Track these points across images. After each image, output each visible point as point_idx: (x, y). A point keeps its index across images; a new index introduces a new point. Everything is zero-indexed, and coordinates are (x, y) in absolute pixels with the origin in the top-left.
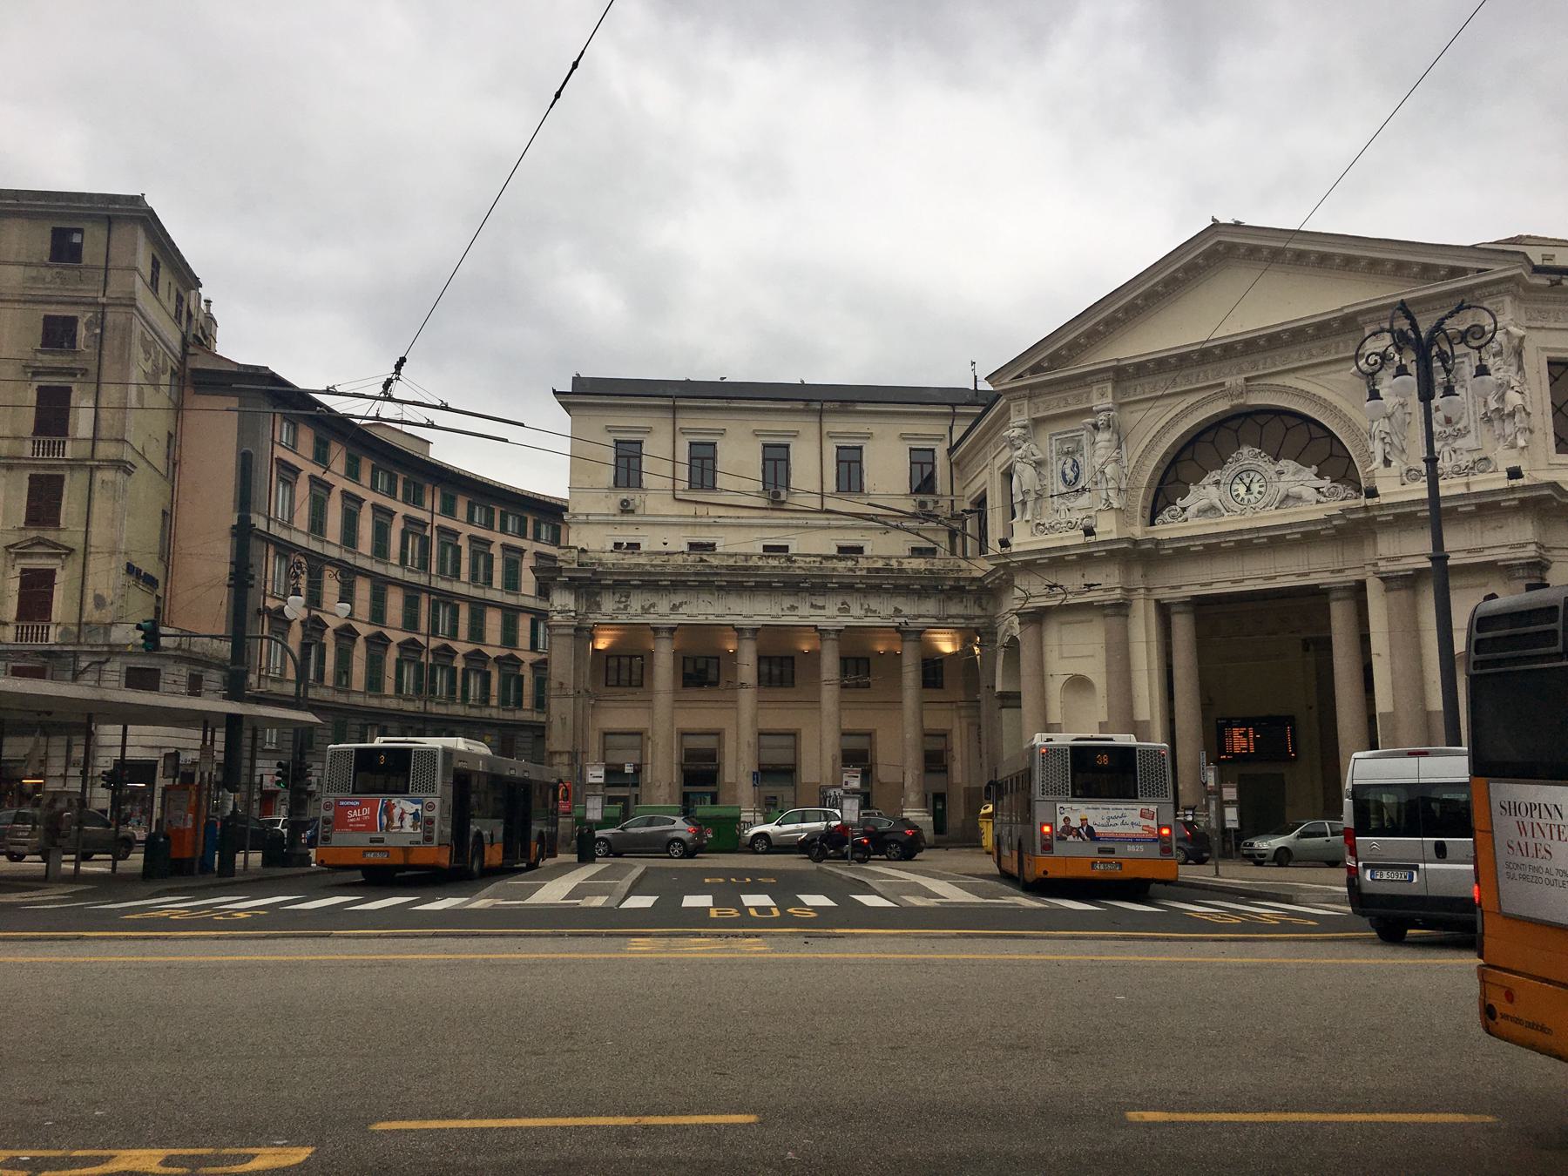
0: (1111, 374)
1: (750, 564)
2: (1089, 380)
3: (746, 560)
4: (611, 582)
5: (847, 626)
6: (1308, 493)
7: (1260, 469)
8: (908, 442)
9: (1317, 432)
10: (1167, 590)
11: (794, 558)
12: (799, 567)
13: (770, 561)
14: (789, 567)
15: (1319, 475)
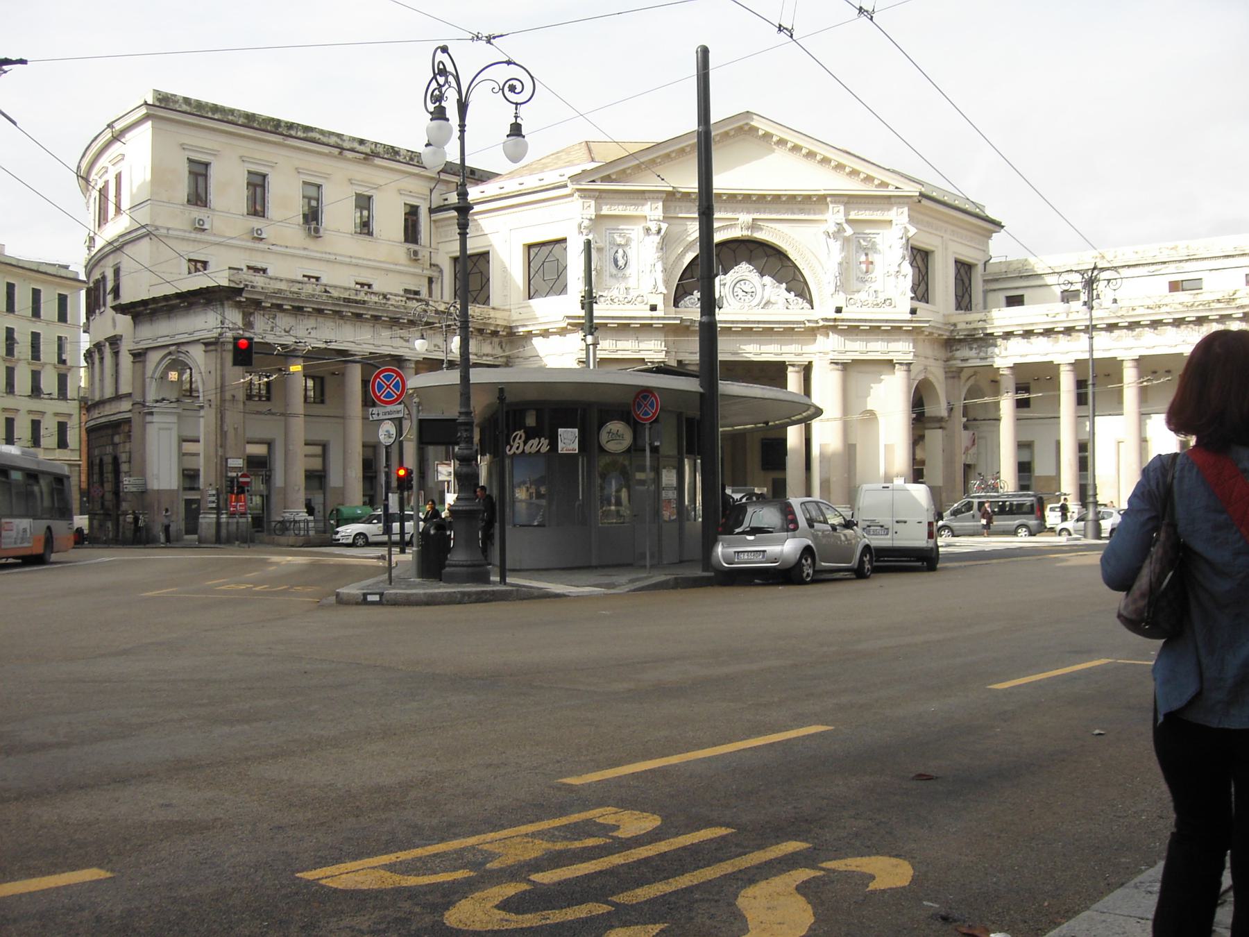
0: (664, 195)
1: (358, 298)
2: (647, 195)
3: (357, 294)
4: (269, 305)
5: (424, 358)
6: (781, 302)
7: (744, 278)
8: (403, 197)
9: (733, 246)
10: (687, 354)
11: (388, 296)
12: (392, 305)
13: (373, 297)
14: (385, 304)
15: (788, 290)
